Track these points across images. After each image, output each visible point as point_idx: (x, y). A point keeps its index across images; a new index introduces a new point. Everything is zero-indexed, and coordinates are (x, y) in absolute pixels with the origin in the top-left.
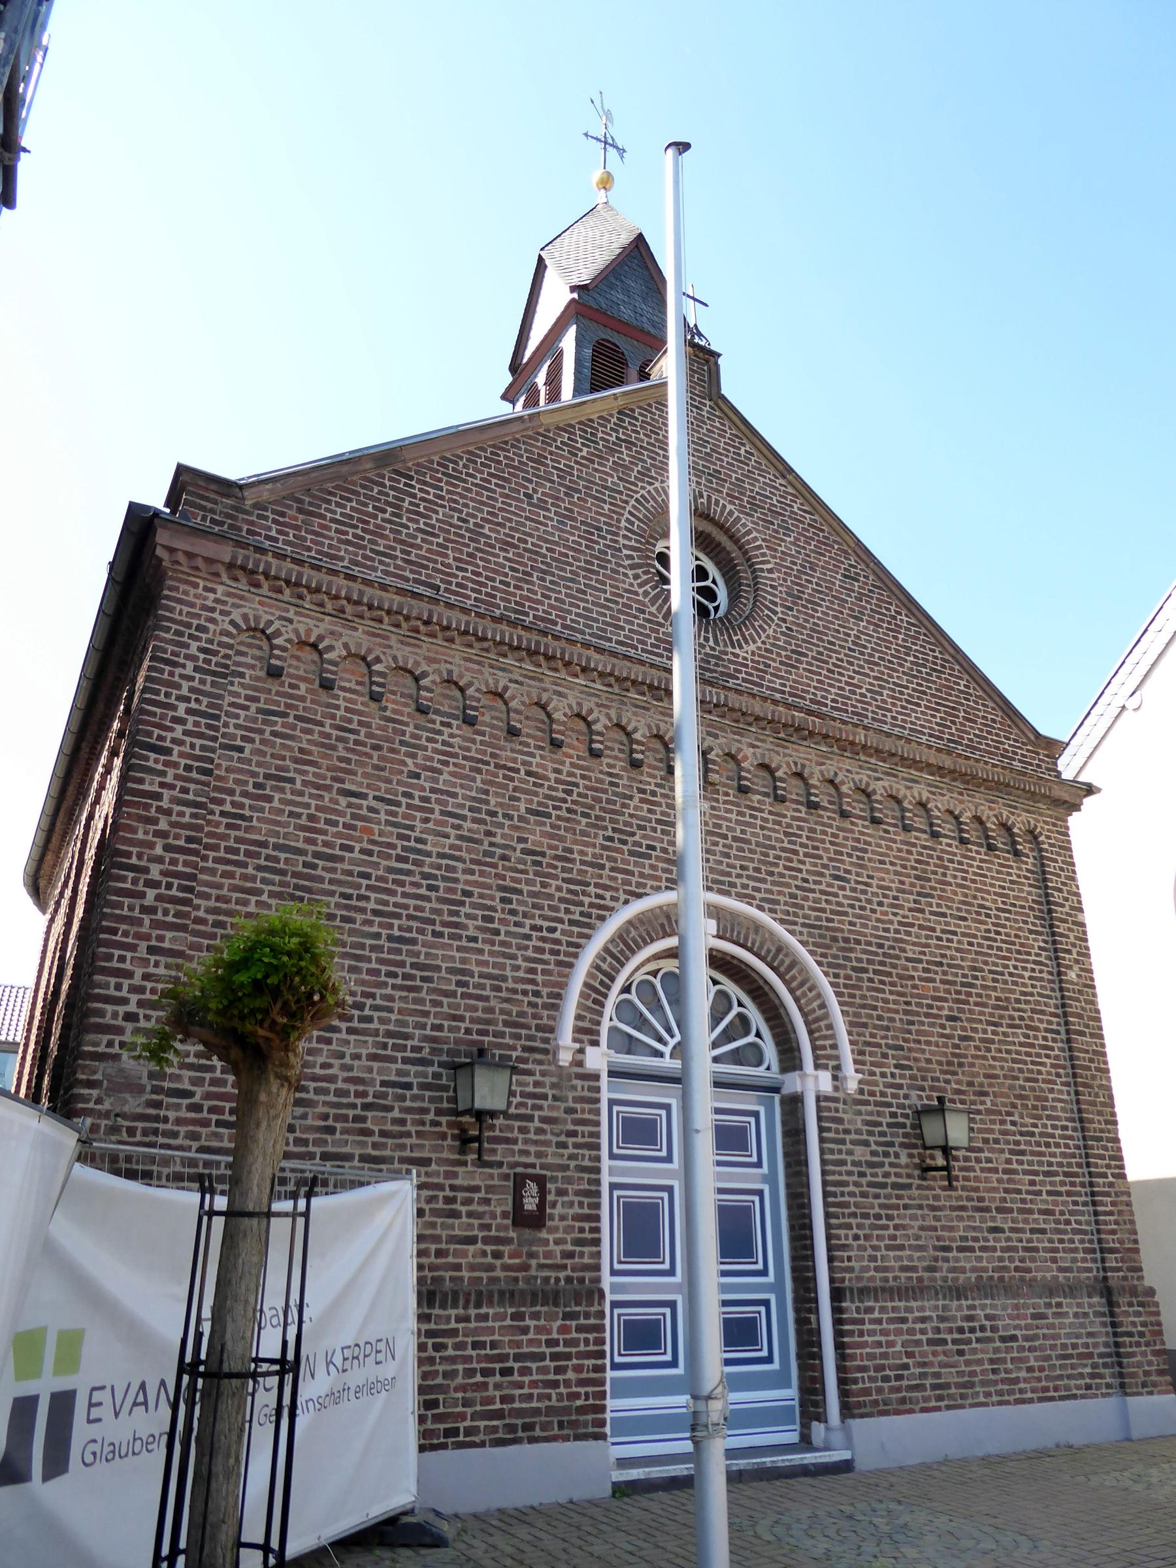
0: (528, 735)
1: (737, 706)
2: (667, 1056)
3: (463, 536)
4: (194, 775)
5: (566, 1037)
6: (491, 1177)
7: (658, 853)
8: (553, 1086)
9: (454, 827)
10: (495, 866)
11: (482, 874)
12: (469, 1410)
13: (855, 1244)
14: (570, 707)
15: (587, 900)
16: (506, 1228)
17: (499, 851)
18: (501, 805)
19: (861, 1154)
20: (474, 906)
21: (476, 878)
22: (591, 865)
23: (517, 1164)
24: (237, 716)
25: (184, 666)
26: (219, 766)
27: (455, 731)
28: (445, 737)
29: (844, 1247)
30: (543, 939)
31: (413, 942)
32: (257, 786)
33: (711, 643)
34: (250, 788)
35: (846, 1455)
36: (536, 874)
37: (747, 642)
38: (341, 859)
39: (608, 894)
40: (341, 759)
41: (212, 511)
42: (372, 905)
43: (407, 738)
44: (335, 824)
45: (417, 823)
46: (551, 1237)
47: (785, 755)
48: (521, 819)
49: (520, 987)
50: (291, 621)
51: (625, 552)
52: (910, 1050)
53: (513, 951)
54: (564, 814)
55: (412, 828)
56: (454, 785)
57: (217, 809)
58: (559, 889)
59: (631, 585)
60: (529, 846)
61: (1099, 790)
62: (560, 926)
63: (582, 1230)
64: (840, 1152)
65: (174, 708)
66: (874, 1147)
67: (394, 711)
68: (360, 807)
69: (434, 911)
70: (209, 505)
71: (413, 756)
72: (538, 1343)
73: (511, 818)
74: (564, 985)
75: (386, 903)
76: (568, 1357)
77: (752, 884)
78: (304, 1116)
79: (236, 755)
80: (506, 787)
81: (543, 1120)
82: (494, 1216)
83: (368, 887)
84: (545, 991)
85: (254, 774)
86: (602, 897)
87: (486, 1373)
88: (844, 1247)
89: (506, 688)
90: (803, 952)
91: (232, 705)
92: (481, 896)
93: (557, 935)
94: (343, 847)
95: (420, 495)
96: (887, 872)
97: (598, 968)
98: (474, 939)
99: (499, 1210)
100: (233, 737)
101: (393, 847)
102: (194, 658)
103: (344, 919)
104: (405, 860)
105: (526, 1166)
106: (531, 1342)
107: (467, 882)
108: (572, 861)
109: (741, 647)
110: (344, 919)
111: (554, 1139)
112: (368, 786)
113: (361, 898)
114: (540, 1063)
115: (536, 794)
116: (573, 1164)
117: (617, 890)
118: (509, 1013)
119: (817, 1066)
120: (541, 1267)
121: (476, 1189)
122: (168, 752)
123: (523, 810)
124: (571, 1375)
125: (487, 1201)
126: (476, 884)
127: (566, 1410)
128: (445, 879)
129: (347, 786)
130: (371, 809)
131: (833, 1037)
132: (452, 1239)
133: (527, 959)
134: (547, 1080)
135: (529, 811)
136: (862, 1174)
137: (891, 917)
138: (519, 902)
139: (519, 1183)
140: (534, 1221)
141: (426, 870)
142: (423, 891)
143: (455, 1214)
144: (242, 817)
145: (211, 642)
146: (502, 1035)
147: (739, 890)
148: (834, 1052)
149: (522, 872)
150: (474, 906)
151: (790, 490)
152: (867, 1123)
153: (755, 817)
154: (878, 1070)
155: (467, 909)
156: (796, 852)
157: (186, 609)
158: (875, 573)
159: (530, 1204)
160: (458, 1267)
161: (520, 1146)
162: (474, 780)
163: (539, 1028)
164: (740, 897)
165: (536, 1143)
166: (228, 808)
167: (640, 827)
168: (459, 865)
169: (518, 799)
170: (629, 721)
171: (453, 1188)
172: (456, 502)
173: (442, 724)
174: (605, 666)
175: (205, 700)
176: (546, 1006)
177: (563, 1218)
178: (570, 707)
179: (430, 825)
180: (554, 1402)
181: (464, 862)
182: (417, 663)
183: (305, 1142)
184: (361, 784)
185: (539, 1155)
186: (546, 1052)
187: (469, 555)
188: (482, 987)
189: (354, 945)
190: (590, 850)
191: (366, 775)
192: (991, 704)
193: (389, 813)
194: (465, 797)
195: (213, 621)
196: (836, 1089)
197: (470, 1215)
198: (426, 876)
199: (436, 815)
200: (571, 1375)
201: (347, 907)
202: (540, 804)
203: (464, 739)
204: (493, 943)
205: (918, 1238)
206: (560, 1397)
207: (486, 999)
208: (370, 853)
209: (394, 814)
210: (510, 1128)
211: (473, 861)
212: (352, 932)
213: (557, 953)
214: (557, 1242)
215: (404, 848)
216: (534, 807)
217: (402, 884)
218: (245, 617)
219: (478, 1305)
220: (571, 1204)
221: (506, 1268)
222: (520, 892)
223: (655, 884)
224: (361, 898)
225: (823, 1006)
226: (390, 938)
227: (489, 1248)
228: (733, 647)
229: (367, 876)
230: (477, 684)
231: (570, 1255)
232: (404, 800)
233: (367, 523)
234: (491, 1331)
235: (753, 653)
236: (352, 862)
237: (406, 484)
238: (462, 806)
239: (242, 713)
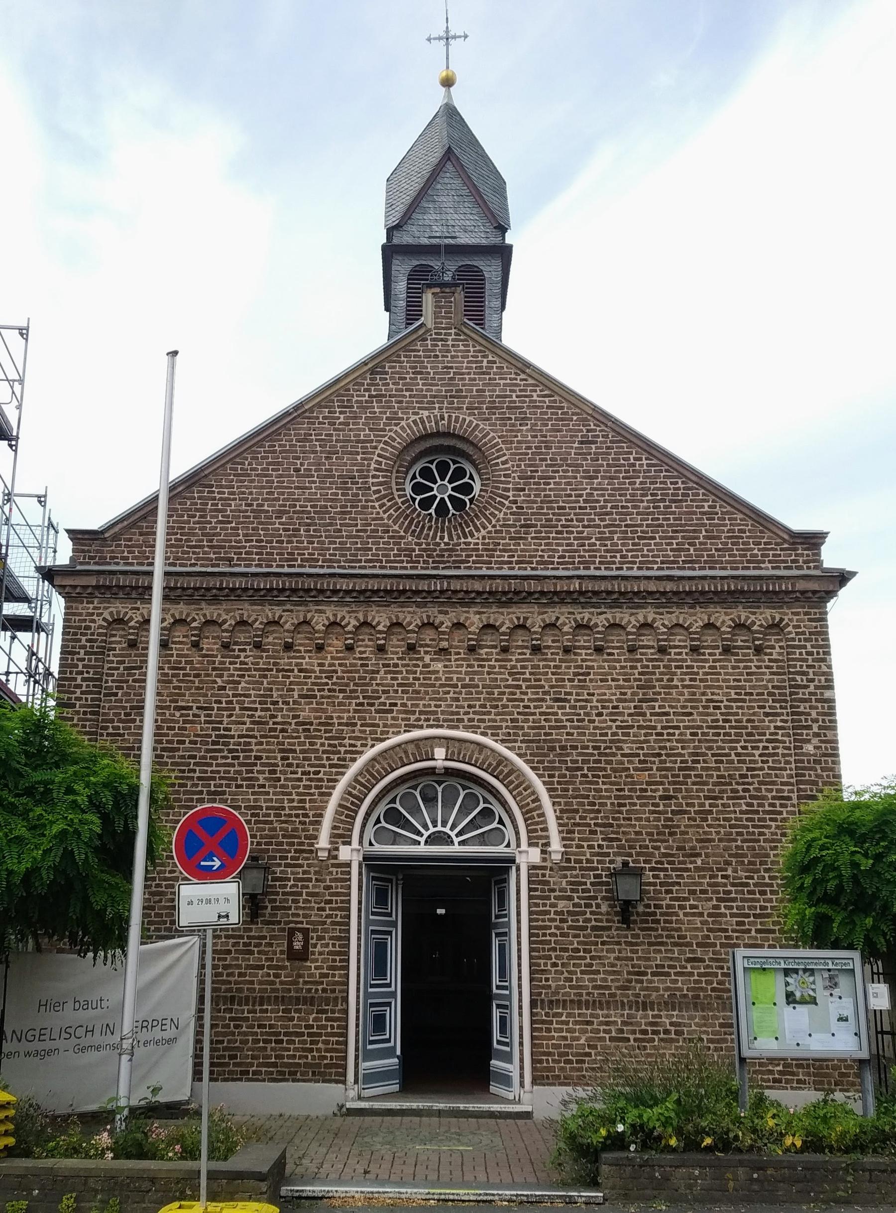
0: (300, 645)
1: (458, 588)
2: (423, 843)
3: (249, 517)
4: (89, 716)
5: (323, 842)
6: (274, 930)
7: (399, 708)
8: (316, 873)
9: (248, 716)
10: (277, 737)
11: (268, 743)
12: (256, 1062)
13: (553, 969)
14: (328, 618)
15: (342, 749)
16: (283, 960)
17: (279, 727)
18: (281, 696)
19: (562, 905)
20: (262, 765)
21: (264, 746)
22: (347, 725)
23: (292, 922)
24: (113, 675)
25: (79, 653)
26: (104, 707)
27: (248, 653)
28: (242, 659)
29: (543, 972)
30: (311, 780)
31: (224, 793)
32: (126, 714)
33: (446, 540)
34: (122, 716)
35: (529, 1109)
36: (306, 737)
37: (478, 530)
38: (178, 749)
39: (359, 743)
40: (175, 688)
41: (89, 551)
42: (197, 774)
43: (217, 665)
44: (173, 728)
45: (225, 719)
46: (313, 965)
47: (508, 614)
48: (294, 702)
49: (294, 812)
50: (138, 609)
51: (373, 488)
52: (619, 826)
53: (290, 790)
54: (326, 693)
55: (221, 722)
56: (249, 689)
57: (105, 732)
58: (322, 745)
59: (378, 513)
60: (301, 720)
61: (853, 574)
62: (322, 770)
63: (335, 961)
64: (545, 905)
65: (75, 679)
66: (576, 900)
67: (208, 650)
68: (188, 715)
69: (236, 772)
70: (86, 548)
71: (221, 676)
72: (300, 1027)
73: (288, 703)
74: (324, 808)
75: (206, 772)
76: (320, 1035)
77: (477, 717)
78: (160, 901)
79: (113, 698)
80: (284, 683)
81: (308, 894)
82: (275, 953)
83: (195, 764)
84: (311, 813)
85: (125, 708)
86: (355, 746)
87: (265, 1041)
88: (543, 972)
89: (281, 617)
90: (520, 762)
91: (110, 669)
92: (267, 758)
93: (321, 775)
94: (179, 742)
95: (218, 496)
96: (610, 687)
97: (350, 794)
98: (263, 786)
99: (278, 949)
100: (111, 688)
101: (210, 736)
102: (84, 647)
103: (181, 785)
104: (217, 743)
105: (297, 923)
106: (295, 1026)
107: (258, 751)
108: (332, 724)
109: (472, 536)
110: (181, 785)
111: (316, 906)
112: (193, 701)
113: (190, 771)
114: (307, 859)
115: (306, 684)
116: (329, 921)
117: (366, 739)
118: (286, 830)
119: (530, 845)
120: (305, 983)
121: (265, 938)
122: (74, 706)
123: (296, 696)
124: (320, 1045)
125: (271, 945)
126: (264, 751)
127: (319, 1065)
128: (243, 751)
129: (180, 704)
130: (194, 715)
131: (545, 822)
132: (248, 967)
133: (298, 794)
134: (312, 870)
135: (300, 696)
136: (563, 921)
137: (609, 723)
138: (294, 758)
139: (292, 933)
140: (302, 956)
141: (231, 747)
142: (229, 761)
143: (251, 953)
144: (119, 735)
145: (93, 634)
146: (281, 844)
147: (466, 723)
148: (544, 834)
149: (296, 738)
150: (262, 765)
151: (531, 381)
152: (571, 883)
153: (484, 666)
154: (585, 844)
155: (259, 768)
156: (519, 687)
157: (77, 618)
158: (614, 430)
159: (298, 945)
160: (252, 982)
161: (293, 911)
162: (262, 683)
163: (306, 837)
164: (466, 728)
165: (304, 908)
166: (111, 731)
167: (384, 692)
168: (254, 740)
169: (293, 690)
170: (374, 618)
171: (248, 937)
172: (244, 493)
173: (240, 650)
174: (348, 585)
175: (92, 671)
176: (311, 823)
177: (320, 954)
178: (328, 618)
179: (233, 718)
180: (309, 1060)
181: (256, 738)
182: (219, 615)
183: (161, 915)
184: (188, 701)
185: (305, 916)
186: (311, 852)
187: (253, 529)
188: (269, 815)
189: (187, 800)
190: (345, 715)
191: (192, 695)
192: (740, 516)
193: (206, 716)
194: (256, 696)
195: (94, 621)
196: (544, 860)
197: (259, 952)
198: (230, 751)
199: (237, 711)
200: (320, 1045)
201: (182, 778)
202: (308, 690)
203: (255, 657)
204: (275, 787)
205: (613, 965)
206: (314, 1057)
207: (271, 822)
208: (195, 743)
209: (210, 716)
210: (287, 901)
211: (261, 736)
212: (185, 793)
213: (321, 787)
214: (316, 968)
215: (217, 736)
216: (305, 692)
217: (216, 758)
218: (111, 613)
219: (261, 1004)
220: (327, 945)
221: (282, 983)
222: (294, 751)
223: (395, 730)
224: (190, 771)
225: (537, 800)
226: (209, 793)
227: (271, 972)
228: (465, 537)
229: (194, 757)
230: (260, 619)
231: (326, 975)
232: (215, 706)
233: (183, 528)
234: (270, 1019)
235: (484, 538)
236: (185, 750)
237: (209, 492)
238: (254, 702)
239: (116, 672)
